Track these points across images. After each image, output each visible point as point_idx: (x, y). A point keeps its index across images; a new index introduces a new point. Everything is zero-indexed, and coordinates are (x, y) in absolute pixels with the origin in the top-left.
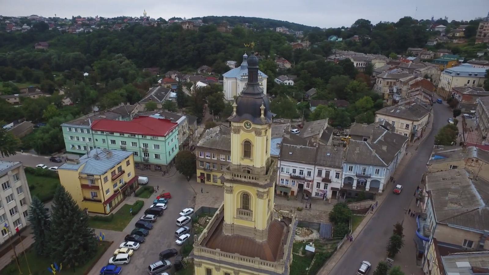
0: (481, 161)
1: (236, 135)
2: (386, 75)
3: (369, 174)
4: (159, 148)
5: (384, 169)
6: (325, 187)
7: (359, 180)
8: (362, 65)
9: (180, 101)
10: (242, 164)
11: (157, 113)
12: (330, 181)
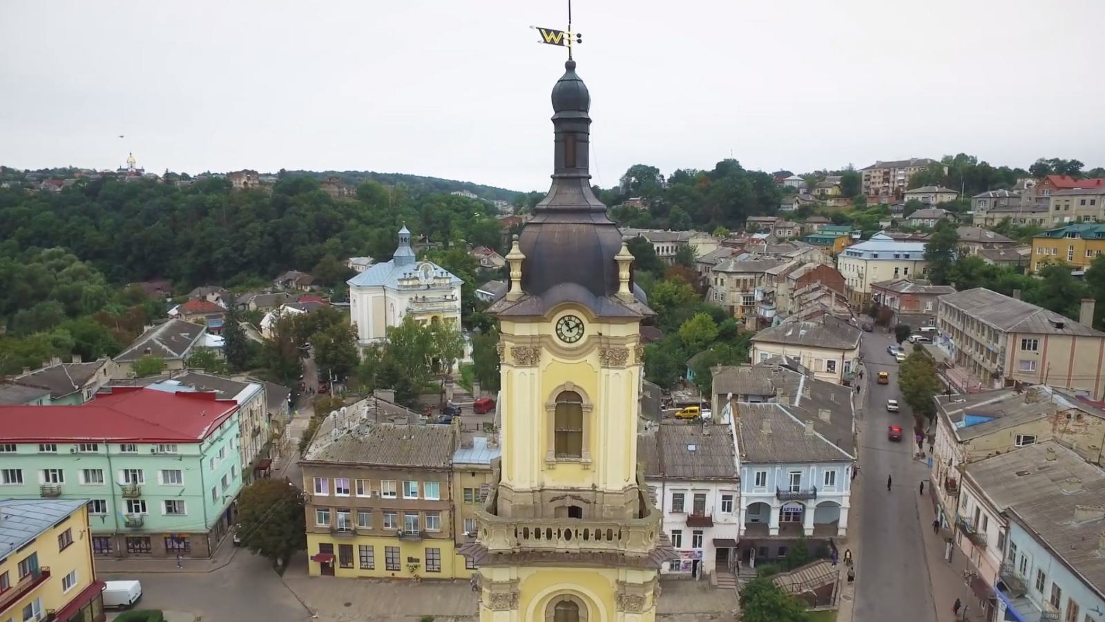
0: (1089, 414)
1: (527, 371)
2: (732, 265)
3: (810, 487)
4: (179, 481)
5: (848, 470)
6: (697, 541)
7: (785, 507)
8: (667, 251)
9: (235, 352)
10: (549, 484)
11: (170, 379)
12: (708, 522)
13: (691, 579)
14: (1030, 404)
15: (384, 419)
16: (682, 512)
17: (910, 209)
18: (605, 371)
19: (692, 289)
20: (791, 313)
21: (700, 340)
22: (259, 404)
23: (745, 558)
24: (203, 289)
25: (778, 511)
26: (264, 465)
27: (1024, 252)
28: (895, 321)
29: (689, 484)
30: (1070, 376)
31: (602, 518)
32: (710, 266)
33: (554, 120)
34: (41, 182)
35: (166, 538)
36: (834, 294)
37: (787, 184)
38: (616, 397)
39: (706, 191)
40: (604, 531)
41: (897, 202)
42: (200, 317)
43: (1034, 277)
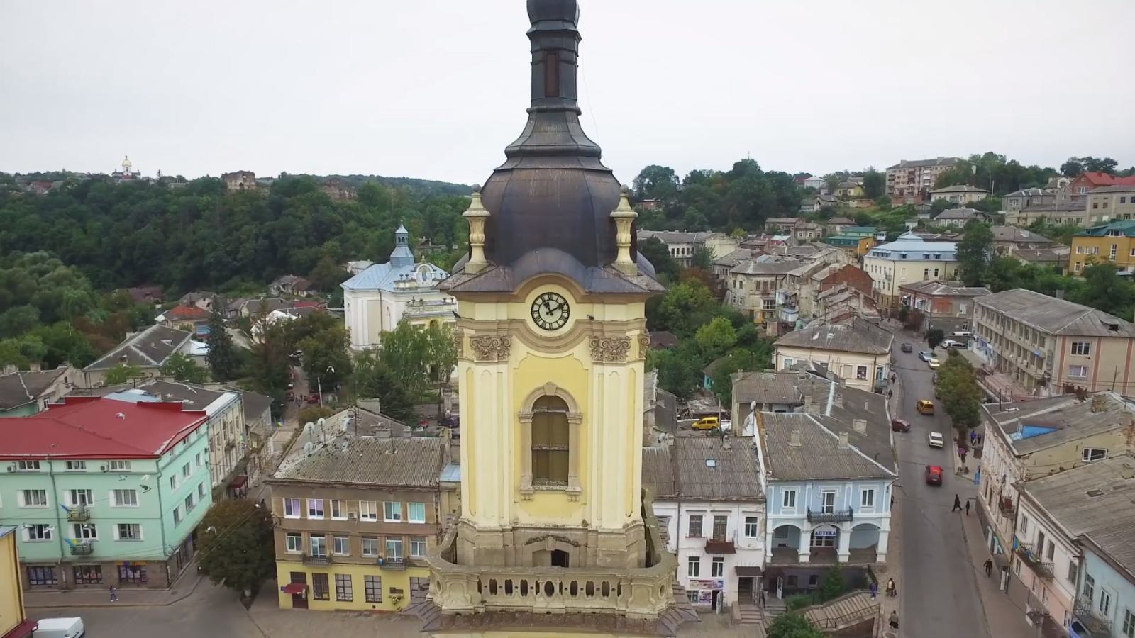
1: (492, 368)
2: (751, 267)
3: (845, 508)
4: (134, 502)
5: (888, 488)
6: (717, 569)
8: (683, 252)
9: (219, 360)
11: (134, 387)
12: (730, 548)
13: (710, 612)
14: (1097, 414)
15: (366, 431)
16: (701, 537)
17: (937, 209)
18: (598, 368)
19: (708, 292)
20: (815, 316)
21: (717, 346)
22: (235, 414)
23: (772, 589)
24: (193, 295)
25: (809, 535)
26: (239, 483)
27: (1061, 251)
28: (926, 326)
29: (708, 504)
30: (1125, 382)
31: (595, 567)
32: (728, 269)
33: (529, 35)
34: (29, 184)
35: (119, 567)
36: (862, 296)
37: (807, 184)
38: (616, 404)
39: (723, 192)
40: (598, 584)
41: (923, 202)
42: (186, 323)
43: (1075, 278)
